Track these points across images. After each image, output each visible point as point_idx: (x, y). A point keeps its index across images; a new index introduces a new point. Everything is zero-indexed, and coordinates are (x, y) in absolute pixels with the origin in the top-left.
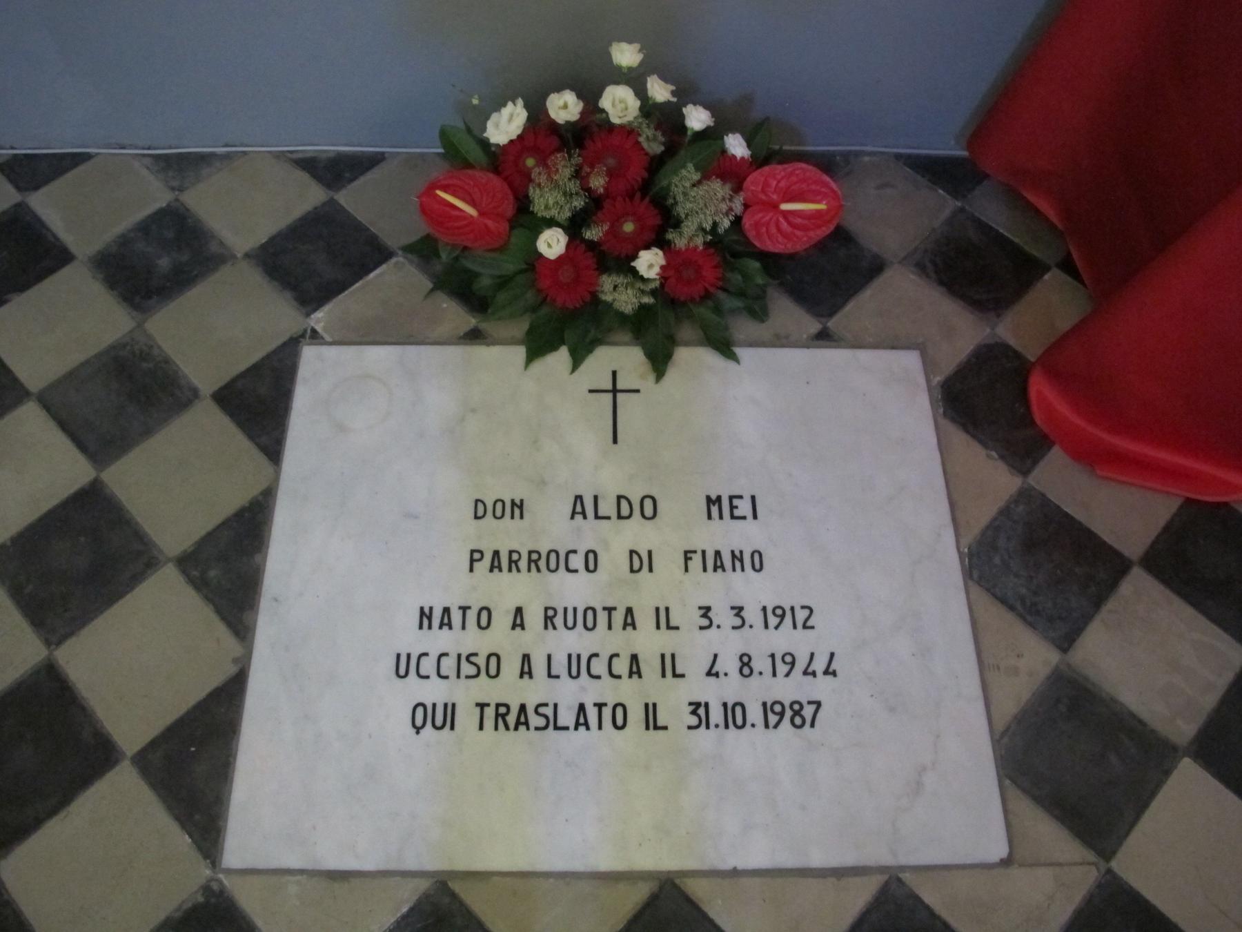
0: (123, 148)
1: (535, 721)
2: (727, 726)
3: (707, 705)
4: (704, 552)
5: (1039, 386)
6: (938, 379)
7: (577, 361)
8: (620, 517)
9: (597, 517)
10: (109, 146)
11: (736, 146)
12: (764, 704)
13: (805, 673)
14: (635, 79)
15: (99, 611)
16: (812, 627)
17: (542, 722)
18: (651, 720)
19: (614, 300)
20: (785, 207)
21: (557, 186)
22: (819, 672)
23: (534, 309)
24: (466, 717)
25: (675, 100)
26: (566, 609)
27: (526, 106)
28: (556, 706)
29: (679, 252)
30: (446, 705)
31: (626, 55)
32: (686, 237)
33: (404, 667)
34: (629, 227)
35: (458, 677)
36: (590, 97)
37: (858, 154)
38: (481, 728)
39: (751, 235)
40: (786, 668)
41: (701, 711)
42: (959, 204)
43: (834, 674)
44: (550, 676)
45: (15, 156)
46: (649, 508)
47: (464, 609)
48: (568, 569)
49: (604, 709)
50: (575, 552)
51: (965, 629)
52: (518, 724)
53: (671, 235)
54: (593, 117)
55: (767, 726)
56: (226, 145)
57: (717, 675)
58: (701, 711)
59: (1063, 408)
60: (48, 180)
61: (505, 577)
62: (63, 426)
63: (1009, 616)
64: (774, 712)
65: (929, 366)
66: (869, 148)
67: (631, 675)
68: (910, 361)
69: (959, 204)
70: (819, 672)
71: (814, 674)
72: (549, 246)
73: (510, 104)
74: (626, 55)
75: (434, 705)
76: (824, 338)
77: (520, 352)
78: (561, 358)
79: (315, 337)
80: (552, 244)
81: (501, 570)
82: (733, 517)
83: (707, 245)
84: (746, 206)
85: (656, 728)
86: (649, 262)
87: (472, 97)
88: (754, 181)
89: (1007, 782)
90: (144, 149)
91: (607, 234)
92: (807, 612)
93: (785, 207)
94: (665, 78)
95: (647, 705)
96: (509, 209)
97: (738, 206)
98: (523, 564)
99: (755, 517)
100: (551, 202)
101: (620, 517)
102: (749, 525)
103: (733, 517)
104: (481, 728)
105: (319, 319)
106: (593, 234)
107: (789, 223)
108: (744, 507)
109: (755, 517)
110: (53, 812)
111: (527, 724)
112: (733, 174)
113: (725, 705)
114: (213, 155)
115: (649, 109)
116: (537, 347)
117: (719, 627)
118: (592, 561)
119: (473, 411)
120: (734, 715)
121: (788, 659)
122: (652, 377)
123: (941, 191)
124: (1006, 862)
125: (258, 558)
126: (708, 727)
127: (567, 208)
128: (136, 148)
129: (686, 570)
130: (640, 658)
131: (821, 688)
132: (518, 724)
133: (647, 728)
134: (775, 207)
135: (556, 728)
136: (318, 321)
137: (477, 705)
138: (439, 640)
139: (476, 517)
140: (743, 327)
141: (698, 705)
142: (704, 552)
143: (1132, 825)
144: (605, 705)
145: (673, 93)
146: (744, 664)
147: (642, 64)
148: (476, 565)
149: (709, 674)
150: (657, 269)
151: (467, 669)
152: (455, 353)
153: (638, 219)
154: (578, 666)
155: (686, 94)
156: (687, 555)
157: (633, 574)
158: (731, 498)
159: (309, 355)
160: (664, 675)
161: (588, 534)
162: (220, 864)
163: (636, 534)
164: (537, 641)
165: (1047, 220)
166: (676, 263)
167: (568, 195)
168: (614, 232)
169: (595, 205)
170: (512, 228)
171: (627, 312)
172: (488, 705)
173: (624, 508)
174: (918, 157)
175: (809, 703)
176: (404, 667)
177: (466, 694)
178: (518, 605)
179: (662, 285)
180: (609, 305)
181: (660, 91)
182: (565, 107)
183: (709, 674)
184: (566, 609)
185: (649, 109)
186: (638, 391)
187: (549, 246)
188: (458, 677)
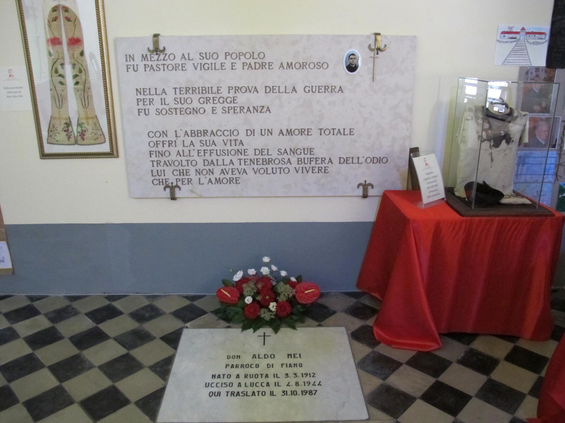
0: (138, 293)
1: (241, 394)
2: (292, 395)
3: (287, 391)
4: (287, 364)
5: (375, 329)
6: (350, 332)
7: (254, 332)
8: (265, 358)
9: (259, 358)
10: (134, 293)
11: (293, 279)
12: (302, 391)
13: (313, 385)
14: (267, 265)
15: (126, 376)
16: (315, 377)
17: (243, 395)
18: (272, 394)
19: (264, 316)
20: (306, 292)
21: (250, 287)
22: (317, 385)
23: (243, 321)
24: (223, 394)
25: (278, 270)
26: (250, 375)
27: (243, 271)
28: (247, 392)
29: (280, 303)
30: (218, 392)
31: (266, 259)
32: (282, 298)
33: (207, 385)
34: (267, 297)
35: (222, 387)
36: (258, 269)
37: (330, 292)
38: (227, 396)
39: (298, 299)
40: (305, 376)
41: (285, 392)
42: (357, 300)
43: (321, 385)
44: (245, 386)
45: (109, 296)
46: (273, 356)
47: (224, 375)
48: (251, 367)
49: (260, 392)
50: (253, 364)
51: (357, 381)
52: (237, 395)
53: (278, 298)
54: (258, 273)
55: (302, 395)
56: (165, 293)
57: (289, 386)
58: (285, 392)
59: (383, 334)
60: (116, 300)
61: (235, 369)
62: (119, 343)
63: (369, 375)
64: (304, 393)
65: (347, 330)
66: (333, 291)
67: (267, 386)
68: (343, 329)
69: (357, 300)
70: (317, 385)
71: (315, 385)
72: (248, 301)
73: (239, 271)
74: (266, 259)
75: (215, 392)
76: (320, 325)
77: (241, 330)
78: (251, 330)
79: (187, 327)
80: (249, 300)
81: (233, 368)
82: (294, 357)
83: (287, 301)
84: (296, 292)
85: (273, 395)
86: (273, 306)
87: (230, 269)
88: (297, 286)
89: (368, 405)
90: (143, 294)
91: (262, 298)
92: (313, 374)
93: (306, 292)
94: (275, 266)
95: (271, 392)
96: (238, 295)
97: (294, 291)
98: (240, 366)
99: (300, 357)
100: (249, 290)
101: (265, 358)
102: (299, 359)
103: (294, 357)
104: (227, 396)
105: (188, 324)
106: (259, 298)
107: (307, 296)
108: (298, 356)
109: (300, 357)
110: (112, 413)
111: (239, 395)
112: (293, 285)
113: (291, 391)
114: (161, 295)
115: (272, 272)
116: (244, 328)
117: (292, 386)
118: (257, 366)
119: (228, 340)
120: (294, 393)
121: (309, 382)
122: (274, 333)
123: (352, 298)
124: (368, 420)
125: (170, 367)
126: (287, 395)
127: (252, 292)
128: (141, 293)
129: (282, 367)
130: (269, 383)
131: (317, 388)
132: (237, 395)
133: (271, 395)
134: (304, 292)
135: (247, 395)
136: (188, 325)
137: (226, 392)
138: (216, 380)
139: (228, 358)
140: (298, 324)
141: (284, 391)
142: (287, 364)
143: (402, 413)
144: (260, 391)
145: (278, 269)
146: (296, 384)
147: (270, 261)
148: (227, 367)
149: (287, 385)
150: (275, 307)
151: (224, 385)
152: (223, 330)
153: (269, 295)
154: (252, 385)
155: (280, 269)
156: (282, 365)
157: (268, 368)
158: (294, 354)
159: (185, 331)
160: (274, 377)
161: (257, 361)
162: (156, 421)
163: (269, 361)
164: (242, 380)
165: (378, 299)
166: (279, 307)
167: (252, 289)
168: (264, 298)
169: (258, 293)
170: (239, 300)
171: (268, 320)
172: (229, 392)
173: (266, 356)
174: (346, 292)
175: (314, 390)
176: (207, 385)
177: (223, 390)
178: (238, 374)
179: (276, 313)
180: (263, 318)
181: (274, 268)
182: (252, 271)
183: (287, 385)
184: (250, 375)
185: (272, 272)
186: (270, 336)
187: (248, 301)
188: (222, 387)
